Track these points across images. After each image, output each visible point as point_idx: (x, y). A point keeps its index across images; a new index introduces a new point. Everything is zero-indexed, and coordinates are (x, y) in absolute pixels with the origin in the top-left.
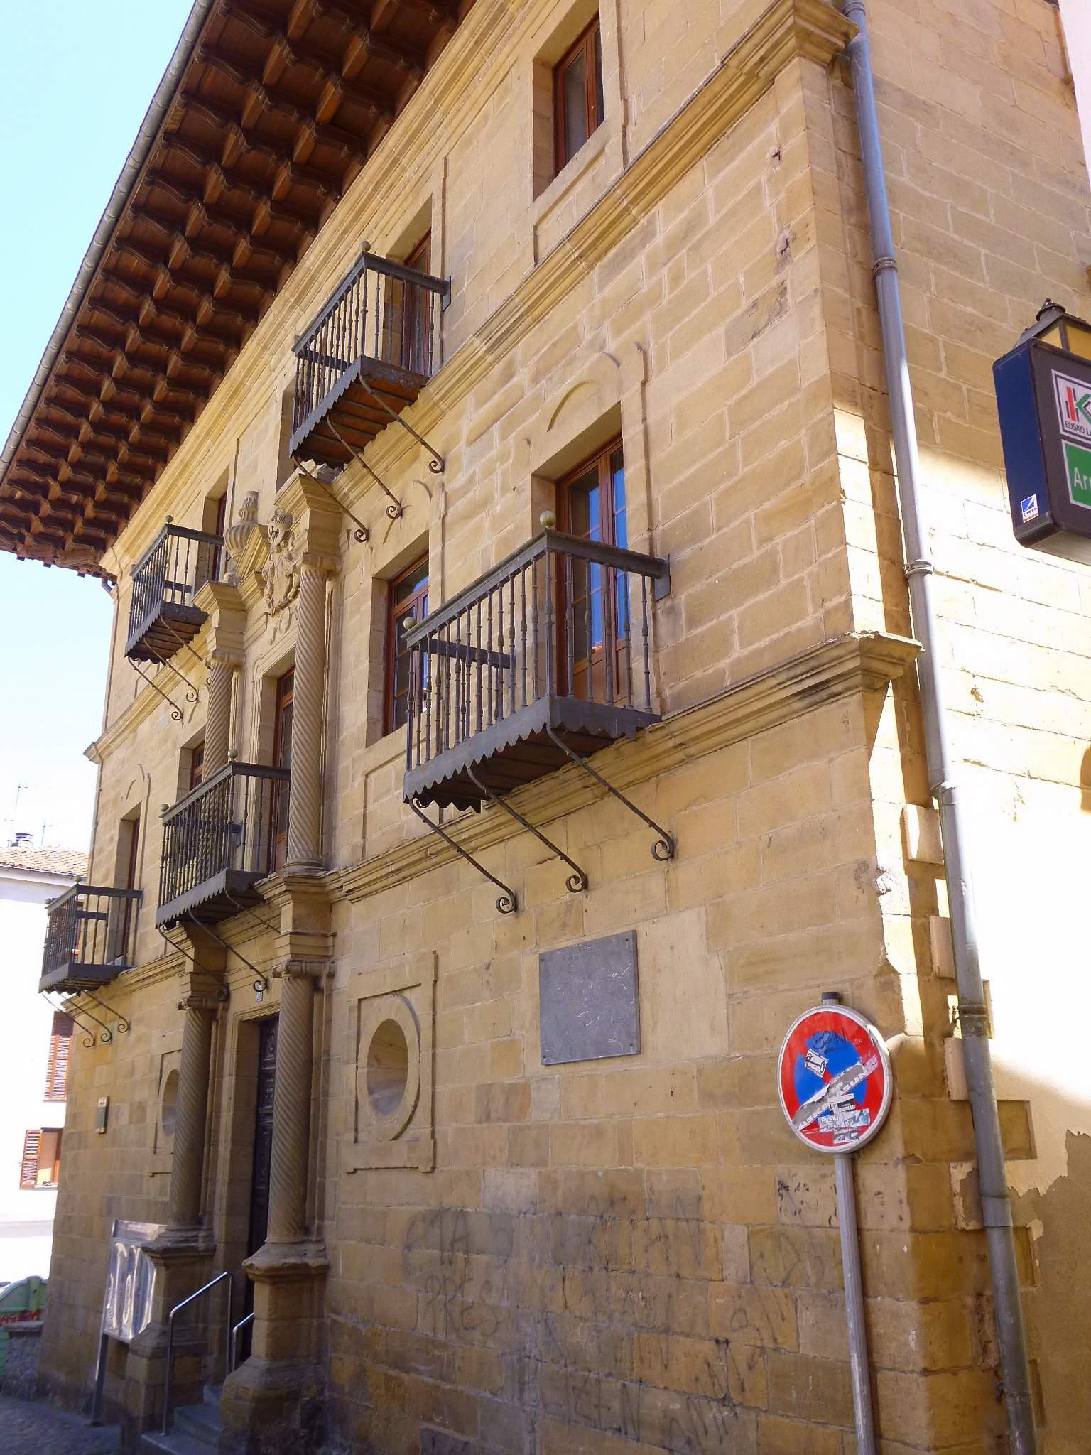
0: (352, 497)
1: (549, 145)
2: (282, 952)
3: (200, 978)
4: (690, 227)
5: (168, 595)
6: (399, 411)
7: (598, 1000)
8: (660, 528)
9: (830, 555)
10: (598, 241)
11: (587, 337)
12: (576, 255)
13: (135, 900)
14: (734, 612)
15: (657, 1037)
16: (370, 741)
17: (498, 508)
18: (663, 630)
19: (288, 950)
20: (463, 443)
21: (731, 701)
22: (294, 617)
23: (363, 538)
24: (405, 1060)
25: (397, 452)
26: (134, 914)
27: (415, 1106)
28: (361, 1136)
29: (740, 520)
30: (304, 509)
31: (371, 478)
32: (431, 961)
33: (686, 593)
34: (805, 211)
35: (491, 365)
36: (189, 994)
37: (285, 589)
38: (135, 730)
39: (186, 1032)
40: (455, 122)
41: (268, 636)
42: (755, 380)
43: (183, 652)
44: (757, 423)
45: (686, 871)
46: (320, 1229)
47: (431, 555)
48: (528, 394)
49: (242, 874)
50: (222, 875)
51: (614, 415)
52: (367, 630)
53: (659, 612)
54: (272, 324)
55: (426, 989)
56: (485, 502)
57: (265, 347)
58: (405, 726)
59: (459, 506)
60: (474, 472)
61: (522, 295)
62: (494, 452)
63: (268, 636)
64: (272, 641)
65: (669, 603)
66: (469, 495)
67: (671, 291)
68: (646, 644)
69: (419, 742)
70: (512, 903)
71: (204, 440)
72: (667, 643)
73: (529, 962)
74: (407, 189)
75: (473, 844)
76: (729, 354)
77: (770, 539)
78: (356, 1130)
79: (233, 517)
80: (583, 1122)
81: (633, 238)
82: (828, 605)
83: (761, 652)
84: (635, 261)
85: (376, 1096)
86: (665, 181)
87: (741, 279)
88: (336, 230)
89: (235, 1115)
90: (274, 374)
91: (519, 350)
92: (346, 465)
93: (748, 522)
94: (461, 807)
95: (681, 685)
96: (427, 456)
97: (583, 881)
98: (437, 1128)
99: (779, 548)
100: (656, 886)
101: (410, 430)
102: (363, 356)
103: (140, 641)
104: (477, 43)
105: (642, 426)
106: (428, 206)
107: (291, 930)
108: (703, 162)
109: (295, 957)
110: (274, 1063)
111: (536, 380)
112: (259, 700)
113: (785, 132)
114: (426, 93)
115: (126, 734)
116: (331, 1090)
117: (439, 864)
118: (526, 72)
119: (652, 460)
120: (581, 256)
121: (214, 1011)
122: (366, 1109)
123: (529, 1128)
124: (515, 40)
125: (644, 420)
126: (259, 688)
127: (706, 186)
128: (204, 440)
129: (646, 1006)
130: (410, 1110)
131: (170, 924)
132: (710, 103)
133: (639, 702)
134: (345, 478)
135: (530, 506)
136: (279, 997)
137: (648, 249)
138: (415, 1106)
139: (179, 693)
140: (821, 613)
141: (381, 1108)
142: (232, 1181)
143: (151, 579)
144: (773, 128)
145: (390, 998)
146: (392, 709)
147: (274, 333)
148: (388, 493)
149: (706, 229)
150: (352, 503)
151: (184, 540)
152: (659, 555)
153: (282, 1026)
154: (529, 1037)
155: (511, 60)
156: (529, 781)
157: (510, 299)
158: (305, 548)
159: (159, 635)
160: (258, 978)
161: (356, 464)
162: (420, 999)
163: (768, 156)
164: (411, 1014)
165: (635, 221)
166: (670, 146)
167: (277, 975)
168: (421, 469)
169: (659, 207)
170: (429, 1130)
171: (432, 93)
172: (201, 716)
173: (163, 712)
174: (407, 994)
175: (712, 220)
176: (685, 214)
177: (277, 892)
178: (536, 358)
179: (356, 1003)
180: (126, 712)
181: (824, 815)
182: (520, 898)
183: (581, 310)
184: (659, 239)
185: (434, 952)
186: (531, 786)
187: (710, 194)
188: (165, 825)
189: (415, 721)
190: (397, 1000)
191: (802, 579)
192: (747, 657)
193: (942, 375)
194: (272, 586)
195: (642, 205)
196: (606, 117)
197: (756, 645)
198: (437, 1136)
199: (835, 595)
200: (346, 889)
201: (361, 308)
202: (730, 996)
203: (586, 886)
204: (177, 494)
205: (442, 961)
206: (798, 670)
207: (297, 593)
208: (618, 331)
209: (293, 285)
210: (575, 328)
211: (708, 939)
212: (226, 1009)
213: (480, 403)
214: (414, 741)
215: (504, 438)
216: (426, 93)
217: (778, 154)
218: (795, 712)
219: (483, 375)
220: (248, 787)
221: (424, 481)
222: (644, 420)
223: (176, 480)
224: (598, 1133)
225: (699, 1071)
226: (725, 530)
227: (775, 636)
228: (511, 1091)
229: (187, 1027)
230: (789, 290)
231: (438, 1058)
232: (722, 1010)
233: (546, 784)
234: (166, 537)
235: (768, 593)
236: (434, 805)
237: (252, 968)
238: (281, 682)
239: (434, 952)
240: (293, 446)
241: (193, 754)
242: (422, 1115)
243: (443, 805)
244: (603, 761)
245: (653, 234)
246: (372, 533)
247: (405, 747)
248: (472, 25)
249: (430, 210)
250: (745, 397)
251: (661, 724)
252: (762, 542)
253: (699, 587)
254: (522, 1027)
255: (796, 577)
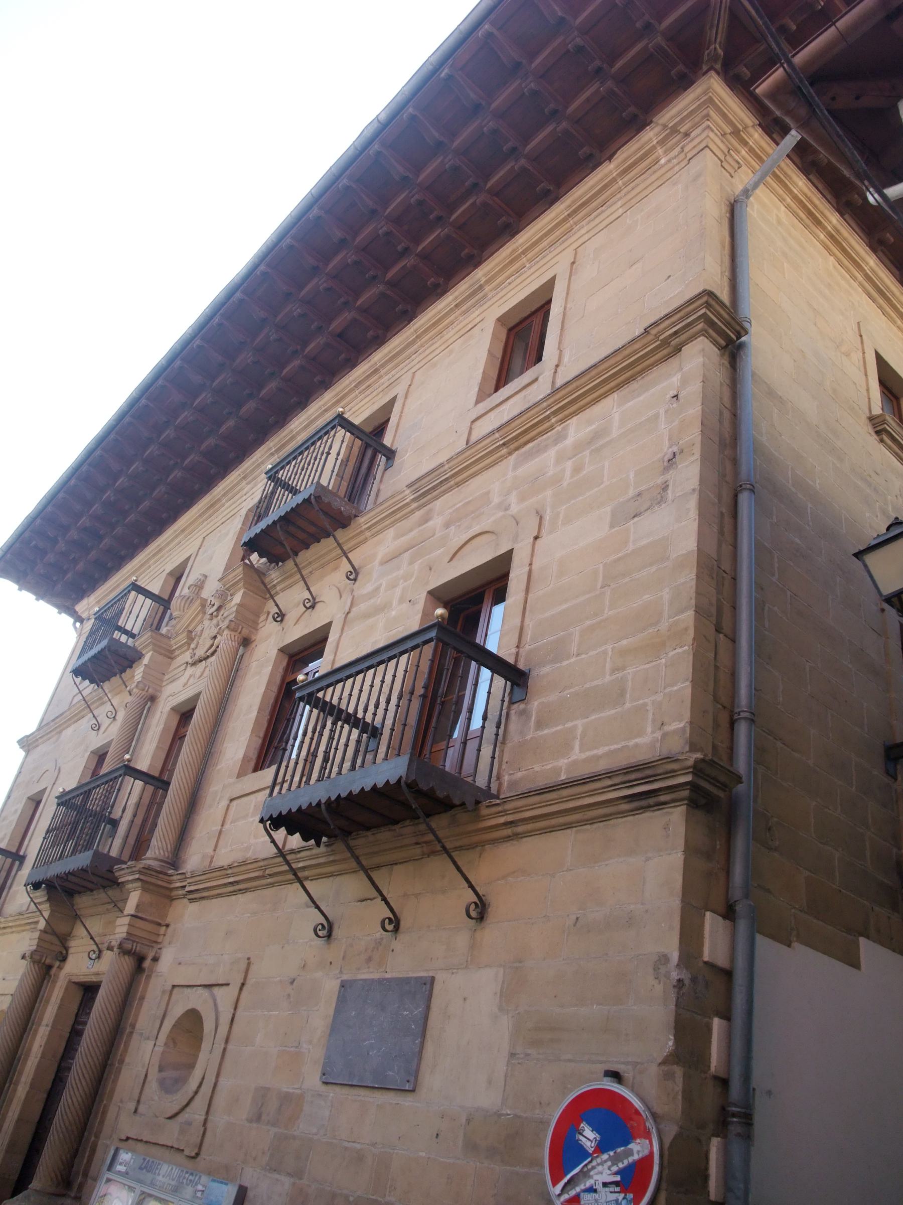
0: (278, 588)
1: (494, 374)
2: (121, 928)
3: (49, 937)
4: (596, 435)
5: (117, 635)
6: (335, 530)
7: (386, 1032)
8: (527, 647)
9: (675, 688)
10: (518, 437)
11: (496, 500)
12: (501, 442)
13: (17, 863)
14: (580, 723)
15: (433, 1080)
16: (241, 774)
17: (393, 613)
18: (512, 727)
19: (125, 929)
20: (377, 562)
21: (565, 793)
22: (207, 669)
23: (279, 619)
24: (199, 1048)
25: (321, 562)
26: (13, 873)
27: (196, 1093)
28: (141, 1109)
29: (599, 650)
30: (240, 589)
31: (299, 576)
32: (243, 966)
33: (540, 701)
34: (694, 435)
35: (412, 512)
36: (34, 948)
37: (207, 646)
38: (60, 732)
39: (21, 980)
40: (427, 352)
41: (183, 680)
42: (631, 547)
43: (116, 680)
44: (627, 579)
45: (492, 934)
46: (81, 1186)
47: (329, 640)
48: (438, 535)
49: (107, 856)
50: (89, 854)
51: (506, 559)
52: (262, 689)
53: (512, 712)
54: (254, 462)
55: (234, 990)
56: (384, 607)
57: (244, 478)
58: (274, 768)
59: (362, 607)
60: (381, 584)
61: (451, 464)
62: (401, 572)
63: (183, 680)
64: (185, 683)
65: (522, 706)
66: (372, 601)
67: (572, 477)
68: (497, 735)
69: (284, 781)
70: (327, 930)
71: (179, 534)
72: (514, 736)
73: (331, 986)
74: (380, 389)
75: (306, 873)
76: (612, 526)
77: (623, 668)
78: (138, 1102)
79: (183, 590)
80: (346, 1144)
81: (548, 438)
82: (667, 728)
83: (598, 757)
84: (546, 455)
85: (164, 1074)
86: (582, 403)
87: (632, 476)
88: (320, 408)
89: (40, 1062)
90: (245, 497)
91: (438, 504)
92: (280, 564)
93: (605, 652)
94: (305, 838)
95: (519, 775)
96: (345, 567)
97: (394, 924)
98: (210, 1117)
99: (630, 677)
100: (462, 940)
101: (339, 545)
102: (318, 482)
103: (84, 664)
104: (456, 306)
105: (527, 569)
106: (393, 401)
107: (133, 912)
108: (615, 395)
109: (130, 936)
110: (85, 1023)
111: (447, 525)
112: (162, 726)
113: (684, 382)
114: (412, 330)
115: (53, 733)
116: (127, 1060)
117: (272, 885)
118: (489, 325)
119: (530, 595)
120: (504, 444)
121: (50, 967)
122: (153, 1085)
123: (294, 1137)
124: (485, 307)
125: (531, 564)
126: (165, 716)
127: (613, 411)
128: (179, 534)
129: (430, 1048)
130: (191, 1094)
131: (36, 886)
132: (629, 356)
133: (481, 781)
134: (277, 573)
135: (420, 615)
136: (107, 969)
137: (560, 446)
138: (196, 1093)
139: (102, 712)
140: (658, 735)
141: (168, 1087)
142: (19, 1120)
143: (107, 621)
144: (676, 380)
145: (200, 990)
146: (271, 746)
147: (253, 470)
148: (308, 589)
149: (608, 439)
150: (277, 593)
151: (141, 598)
152: (521, 666)
153: (102, 993)
154: (314, 1054)
155: (478, 320)
156: (368, 829)
157: (442, 465)
158: (232, 617)
159: (102, 664)
160: (95, 948)
161: (290, 564)
162: (225, 997)
163: (669, 396)
164: (215, 1008)
165: (552, 428)
166: (592, 379)
167: (110, 948)
168: (338, 576)
169: (574, 420)
170: (203, 1117)
171: (416, 331)
172: (112, 732)
173: (87, 722)
174: (216, 990)
175: (615, 433)
176: (594, 427)
177: (131, 878)
178: (451, 511)
179: (170, 988)
180: (57, 718)
181: (632, 907)
182: (335, 927)
183: (497, 483)
184: (569, 441)
185: (249, 959)
186: (369, 833)
187: (616, 417)
188: (58, 805)
189: (284, 764)
190: (205, 993)
191: (645, 705)
192: (584, 761)
193: (774, 579)
194: (198, 643)
195: (561, 416)
196: (544, 359)
197: (595, 752)
198: (209, 1125)
199: (674, 721)
200: (188, 889)
201: (326, 450)
202: (512, 1055)
203: (397, 929)
204: (151, 568)
205: (253, 968)
206: (633, 776)
207: (215, 651)
208: (522, 498)
209: (277, 440)
210: (488, 493)
211: (501, 996)
212: (60, 968)
213: (397, 537)
214: (280, 780)
215: (411, 563)
216: (412, 330)
217: (676, 396)
218: (619, 813)
219: (406, 517)
220: (133, 792)
221: (339, 585)
222: (531, 564)
223: (150, 559)
224: (359, 1158)
225: (468, 1121)
226: (583, 656)
227: (612, 747)
228: (286, 1099)
229: (24, 975)
230: (670, 487)
231: (227, 1054)
232: (501, 1067)
233: (384, 835)
234: (129, 592)
235: (613, 712)
236: (282, 831)
237: (92, 938)
238: (185, 715)
239: (249, 959)
240: (245, 538)
241: (100, 756)
242: (200, 1103)
243: (291, 832)
244: (440, 822)
245: (565, 437)
246: (286, 618)
247: (270, 783)
248: (457, 293)
249: (393, 406)
250: (619, 559)
251: (498, 801)
252: (614, 670)
253: (553, 697)
254: (310, 1042)
255: (641, 702)
